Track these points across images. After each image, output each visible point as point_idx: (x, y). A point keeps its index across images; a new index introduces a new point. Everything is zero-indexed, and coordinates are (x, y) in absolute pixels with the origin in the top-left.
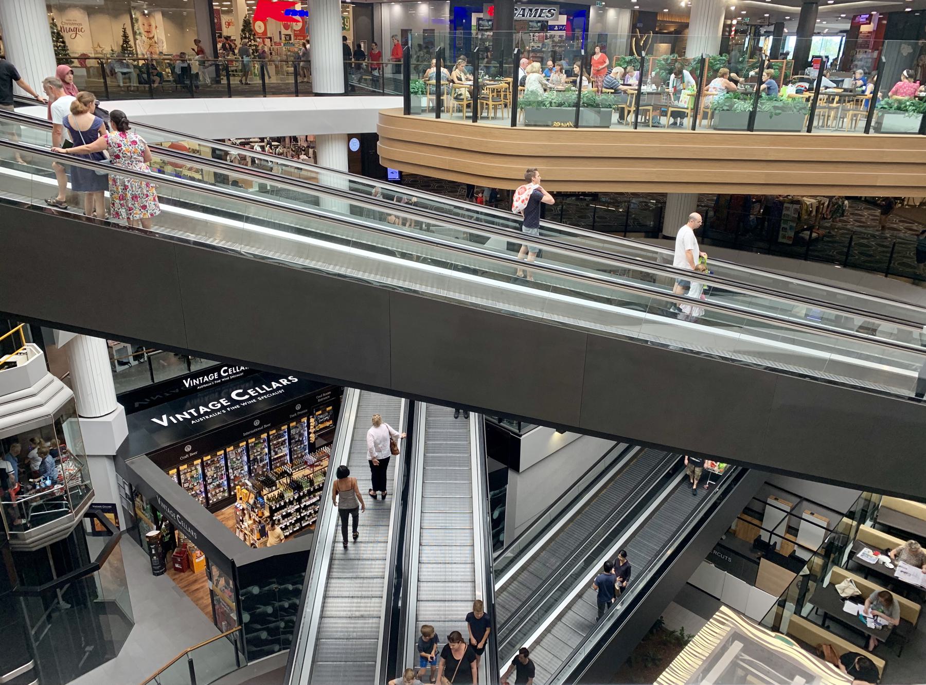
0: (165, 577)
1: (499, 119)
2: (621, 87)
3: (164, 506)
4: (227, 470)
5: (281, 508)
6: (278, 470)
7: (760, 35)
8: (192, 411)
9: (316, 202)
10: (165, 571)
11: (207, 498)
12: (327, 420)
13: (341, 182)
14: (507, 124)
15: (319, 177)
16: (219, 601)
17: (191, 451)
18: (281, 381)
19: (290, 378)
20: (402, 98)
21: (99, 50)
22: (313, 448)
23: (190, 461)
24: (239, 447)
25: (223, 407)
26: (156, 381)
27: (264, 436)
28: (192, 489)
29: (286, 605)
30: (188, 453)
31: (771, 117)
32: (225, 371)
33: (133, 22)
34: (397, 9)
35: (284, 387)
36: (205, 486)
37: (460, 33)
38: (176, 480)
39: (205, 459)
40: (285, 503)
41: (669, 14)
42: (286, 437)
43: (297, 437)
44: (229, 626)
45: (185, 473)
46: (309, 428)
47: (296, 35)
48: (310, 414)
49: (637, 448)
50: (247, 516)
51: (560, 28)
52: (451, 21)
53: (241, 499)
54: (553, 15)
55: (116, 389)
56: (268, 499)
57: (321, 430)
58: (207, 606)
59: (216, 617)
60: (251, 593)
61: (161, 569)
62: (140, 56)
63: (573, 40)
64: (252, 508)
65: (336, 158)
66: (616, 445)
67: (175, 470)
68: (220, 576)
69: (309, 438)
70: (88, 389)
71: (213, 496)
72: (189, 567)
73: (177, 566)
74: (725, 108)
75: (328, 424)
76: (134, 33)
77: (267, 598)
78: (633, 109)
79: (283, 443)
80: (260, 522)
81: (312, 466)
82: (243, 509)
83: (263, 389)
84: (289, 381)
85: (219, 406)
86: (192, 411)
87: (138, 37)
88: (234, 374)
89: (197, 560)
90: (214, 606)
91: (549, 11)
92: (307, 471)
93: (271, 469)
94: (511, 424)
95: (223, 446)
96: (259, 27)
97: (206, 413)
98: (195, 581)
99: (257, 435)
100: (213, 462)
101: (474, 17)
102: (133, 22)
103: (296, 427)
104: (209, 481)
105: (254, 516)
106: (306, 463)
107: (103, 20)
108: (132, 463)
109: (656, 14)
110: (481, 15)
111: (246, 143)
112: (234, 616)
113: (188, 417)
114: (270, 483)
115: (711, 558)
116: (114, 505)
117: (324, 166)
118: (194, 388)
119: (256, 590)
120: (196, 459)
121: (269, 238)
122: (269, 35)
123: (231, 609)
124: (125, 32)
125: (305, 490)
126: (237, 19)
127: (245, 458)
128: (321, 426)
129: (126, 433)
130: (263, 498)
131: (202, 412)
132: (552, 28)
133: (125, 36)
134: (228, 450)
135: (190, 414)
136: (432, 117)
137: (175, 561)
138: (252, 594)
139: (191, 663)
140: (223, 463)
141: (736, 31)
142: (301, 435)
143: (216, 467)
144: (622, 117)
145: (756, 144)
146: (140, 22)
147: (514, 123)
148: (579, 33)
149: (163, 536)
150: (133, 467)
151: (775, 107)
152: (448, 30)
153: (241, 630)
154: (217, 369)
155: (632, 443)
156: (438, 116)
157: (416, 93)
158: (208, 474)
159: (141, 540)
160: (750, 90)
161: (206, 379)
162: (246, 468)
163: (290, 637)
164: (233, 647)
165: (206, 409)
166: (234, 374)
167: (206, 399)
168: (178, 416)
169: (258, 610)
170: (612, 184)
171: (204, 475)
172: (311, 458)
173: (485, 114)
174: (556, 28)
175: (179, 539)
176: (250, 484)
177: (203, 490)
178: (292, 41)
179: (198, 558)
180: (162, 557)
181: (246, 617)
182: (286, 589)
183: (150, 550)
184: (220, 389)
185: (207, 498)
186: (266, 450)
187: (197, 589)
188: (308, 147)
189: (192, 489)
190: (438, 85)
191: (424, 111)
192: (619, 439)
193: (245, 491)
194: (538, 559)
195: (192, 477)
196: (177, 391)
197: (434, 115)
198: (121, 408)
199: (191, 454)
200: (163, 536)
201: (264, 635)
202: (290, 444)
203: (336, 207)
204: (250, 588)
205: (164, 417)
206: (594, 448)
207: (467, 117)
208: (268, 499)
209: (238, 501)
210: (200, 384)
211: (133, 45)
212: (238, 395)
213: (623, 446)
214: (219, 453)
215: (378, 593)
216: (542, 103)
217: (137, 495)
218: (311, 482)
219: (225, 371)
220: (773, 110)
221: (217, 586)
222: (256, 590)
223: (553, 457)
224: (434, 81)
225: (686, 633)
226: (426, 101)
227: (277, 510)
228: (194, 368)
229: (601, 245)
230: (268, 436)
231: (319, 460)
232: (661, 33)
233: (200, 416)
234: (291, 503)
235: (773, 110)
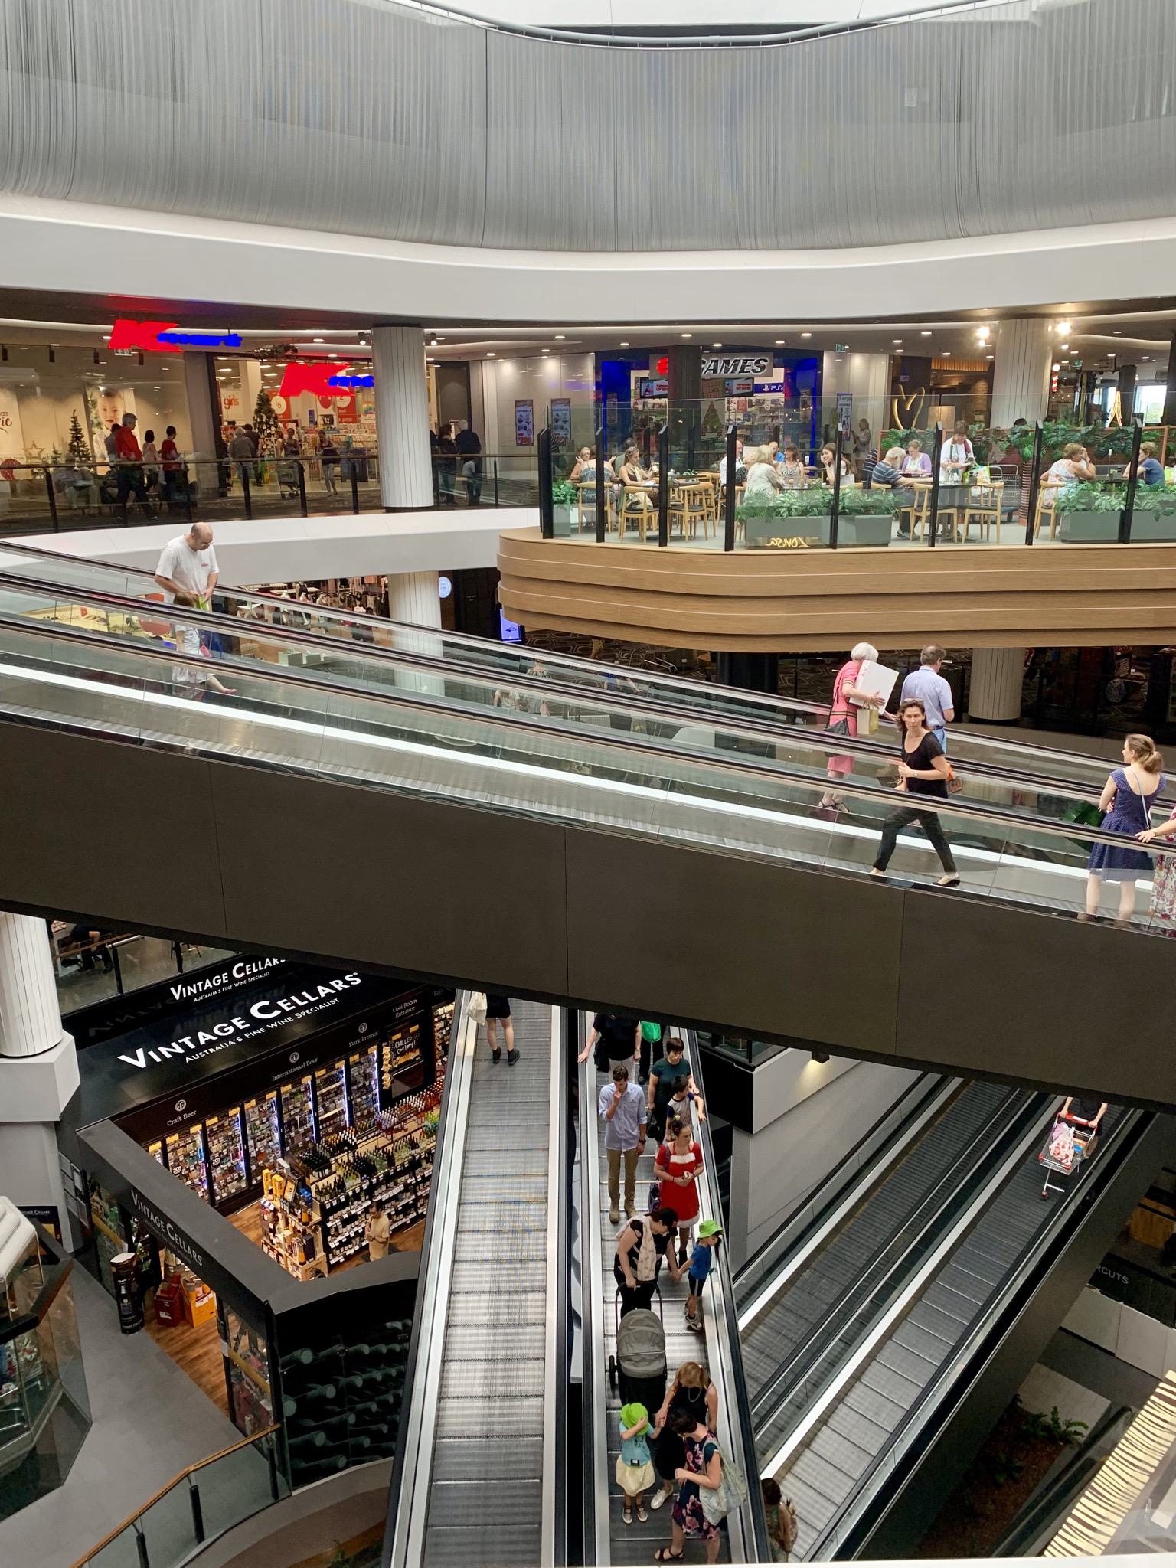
0: (142, 1335)
1: (700, 538)
2: (903, 479)
3: (145, 1209)
4: (245, 1142)
5: (341, 1206)
6: (333, 1139)
7: (1095, 386)
8: (186, 1040)
9: (389, 679)
10: (142, 1325)
11: (212, 1192)
12: (411, 1050)
13: (431, 645)
14: (717, 545)
15: (394, 638)
16: (240, 1378)
18: (333, 983)
19: (347, 978)
20: (537, 511)
21: (35, 452)
22: (388, 1099)
23: (183, 1128)
24: (264, 1100)
25: (238, 1032)
26: (125, 991)
27: (307, 1080)
28: (186, 1176)
29: (359, 1382)
30: (181, 1114)
31: (1157, 519)
32: (239, 971)
33: (89, 406)
34: (508, 369)
35: (338, 994)
36: (209, 1171)
37: (612, 402)
38: (160, 1160)
39: (209, 1123)
40: (347, 1197)
41: (951, 360)
43: (360, 1079)
44: (259, 1423)
45: (175, 1150)
46: (380, 1065)
47: (341, 416)
48: (383, 1039)
49: (957, 1081)
50: (281, 1223)
51: (774, 388)
52: (598, 385)
53: (271, 1192)
54: (763, 368)
55: (61, 1009)
56: (318, 1192)
57: (401, 1066)
58: (216, 1387)
59: (236, 1407)
61: (134, 1321)
62: (99, 460)
63: (797, 407)
64: (291, 1207)
65: (422, 607)
66: (919, 1079)
67: (159, 1145)
68: (242, 1332)
69: (381, 1081)
70: (16, 1005)
71: (222, 1188)
73: (163, 1315)
74: (1080, 507)
75: (412, 1056)
76: (90, 424)
77: (339, 1366)
78: (925, 513)
79: (338, 1092)
80: (304, 1233)
81: (390, 1131)
82: (275, 1211)
83: (303, 999)
84: (346, 982)
85: (231, 1030)
86: (186, 1040)
87: (95, 429)
88: (253, 974)
89: (198, 1304)
90: (230, 1386)
91: (757, 362)
92: (382, 1141)
93: (319, 1139)
94: (735, 1047)
95: (238, 1100)
96: (278, 404)
97: (210, 1044)
98: (196, 1341)
99: (295, 1079)
101: (635, 374)
102: (89, 406)
103: (359, 1063)
104: (216, 1162)
105: (294, 1222)
106: (379, 1125)
107: (40, 407)
108: (89, 1133)
109: (929, 360)
110: (645, 374)
111: (265, 590)
112: (267, 1405)
113: (179, 1050)
114: (319, 1163)
115: (1097, 1281)
116: (54, 1210)
117: (403, 621)
118: (187, 1001)
119: (306, 1356)
121: (331, 744)
122: (294, 417)
123: (262, 1393)
124: (75, 422)
125: (380, 1174)
126: (247, 394)
127: (275, 1120)
128: (401, 1060)
129: (77, 1081)
130: (309, 1190)
131: (202, 1042)
132: (759, 389)
133: (76, 429)
134: (247, 1106)
135: (183, 1045)
136: (591, 539)
137: (159, 1306)
139: (195, 1493)
140: (238, 1128)
141: (1059, 382)
142: (367, 1076)
143: (226, 1137)
144: (905, 527)
145: (1133, 565)
146: (99, 406)
147: (729, 544)
148: (805, 396)
149: (139, 1262)
150: (88, 1140)
151: (1164, 503)
152: (592, 398)
153: (279, 1432)
154: (226, 966)
155: (947, 1072)
156: (600, 539)
157: (562, 502)
158: (214, 1149)
159: (100, 1270)
160: (1117, 477)
162: (277, 1137)
163: (393, 1445)
164: (266, 1463)
165: (209, 1037)
167: (209, 1018)
168: (163, 1050)
169: (310, 1394)
170: (897, 638)
171: (207, 1151)
172: (387, 1117)
173: (675, 532)
174: (766, 389)
175: (167, 1266)
176: (286, 1166)
177: (204, 1177)
178: (335, 425)
179: (199, 1299)
180: (136, 1298)
181: (290, 1407)
182: (359, 1353)
183: (118, 1287)
184: (232, 1002)
185: (212, 1192)
186: (310, 1105)
187: (199, 1357)
188: (366, 593)
189: (186, 1176)
190: (600, 488)
191: (575, 531)
192: (924, 1067)
193: (278, 1178)
194: (798, 1284)
195: (187, 1155)
196: (160, 1006)
197: (594, 536)
198: (70, 1039)
199: (186, 1116)
200: (139, 1262)
201: (320, 1439)
202: (349, 1094)
203: (426, 683)
204: (296, 1353)
205: (140, 1052)
206: (880, 1085)
207: (649, 539)
208: (318, 1192)
209: (267, 1196)
210: (199, 994)
211: (88, 443)
212: (261, 1010)
213: (933, 1078)
214: (231, 1113)
215: (537, 1352)
216: (774, 511)
217: (93, 1190)
218: (391, 1160)
219: (239, 971)
220: (1159, 507)
221: (236, 1349)
222: (306, 1356)
223: (812, 1102)
224: (593, 484)
225: (1062, 1418)
226: (576, 515)
227: (334, 1210)
228: (189, 967)
230: (314, 1081)
231: (402, 1120)
232: (939, 393)
233: (200, 1048)
234: (356, 1197)
235: (1159, 507)
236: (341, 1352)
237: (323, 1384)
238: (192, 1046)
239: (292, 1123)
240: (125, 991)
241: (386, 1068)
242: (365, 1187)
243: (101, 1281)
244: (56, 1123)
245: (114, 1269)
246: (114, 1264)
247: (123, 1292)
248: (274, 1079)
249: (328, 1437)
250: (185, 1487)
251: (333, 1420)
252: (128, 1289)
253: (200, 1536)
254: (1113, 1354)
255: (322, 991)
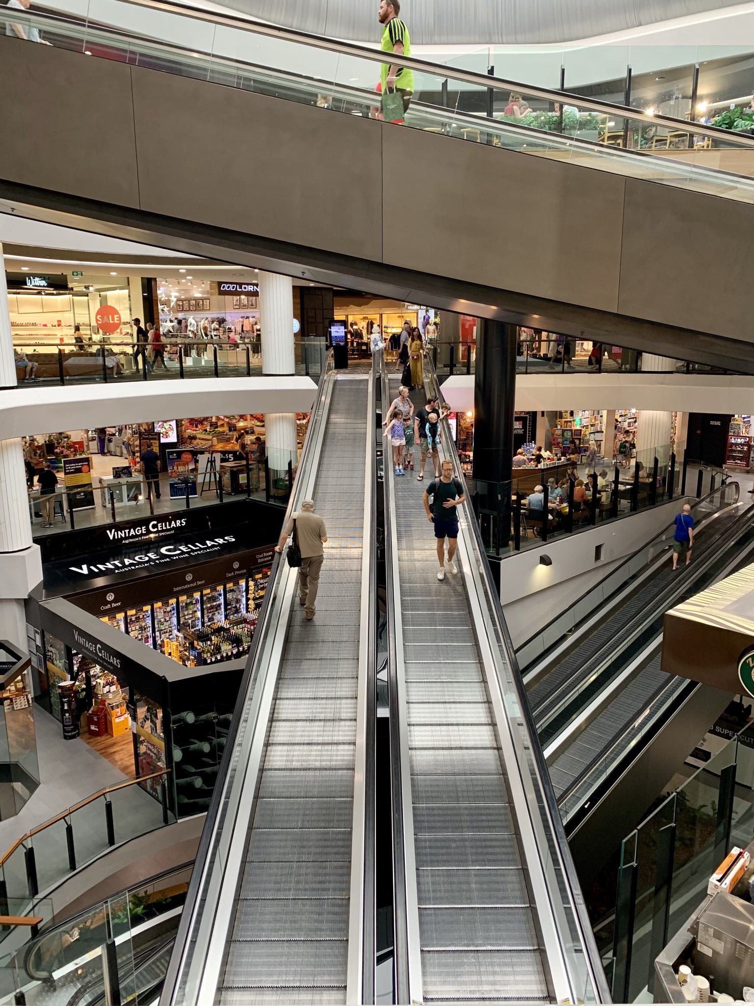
0: (78, 740)
3: (82, 641)
8: (116, 562)
10: (78, 734)
17: (114, 601)
25: (150, 560)
26: (76, 528)
27: (197, 595)
30: (110, 603)
32: (154, 526)
35: (219, 545)
40: (222, 657)
42: (222, 601)
46: (247, 594)
48: (249, 576)
55: (33, 531)
60: (183, 720)
61: (73, 730)
72: (107, 731)
73: (93, 728)
86: (116, 562)
88: (163, 531)
89: (117, 720)
97: (131, 565)
98: (114, 744)
100: (138, 619)
119: (190, 718)
120: (119, 612)
127: (174, 620)
131: (127, 563)
134: (156, 606)
135: (114, 565)
137: (90, 721)
138: (186, 723)
139: (109, 807)
140: (149, 621)
159: (51, 705)
161: (132, 532)
164: (160, 807)
165: (131, 561)
166: (163, 531)
169: (192, 747)
180: (76, 718)
181: (178, 755)
183: (62, 704)
186: (199, 614)
199: (114, 605)
201: (198, 782)
202: (226, 610)
204: (184, 714)
205: (84, 567)
210: (126, 538)
214: (145, 608)
219: (154, 526)
222: (190, 718)
229: (221, 77)
230: (202, 596)
236: (214, 718)
237: (201, 741)
238: (120, 565)
239: (186, 625)
240: (76, 528)
241: (251, 596)
242: (234, 652)
243: (51, 713)
244: (25, 600)
245: (60, 691)
246: (60, 687)
247: (66, 708)
248: (175, 589)
249: (204, 782)
250: (102, 802)
251: (208, 770)
252: (69, 706)
253: (112, 842)
254: (750, 788)
255: (209, 543)
